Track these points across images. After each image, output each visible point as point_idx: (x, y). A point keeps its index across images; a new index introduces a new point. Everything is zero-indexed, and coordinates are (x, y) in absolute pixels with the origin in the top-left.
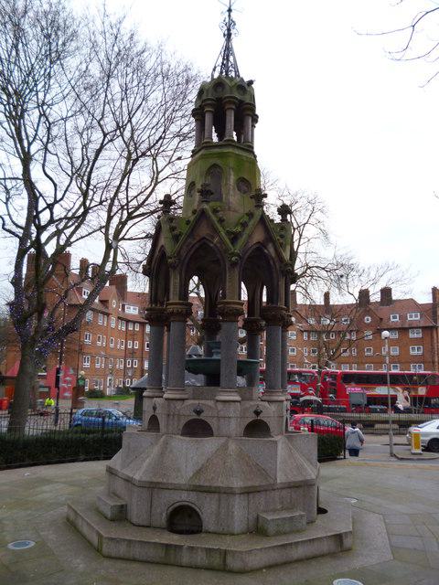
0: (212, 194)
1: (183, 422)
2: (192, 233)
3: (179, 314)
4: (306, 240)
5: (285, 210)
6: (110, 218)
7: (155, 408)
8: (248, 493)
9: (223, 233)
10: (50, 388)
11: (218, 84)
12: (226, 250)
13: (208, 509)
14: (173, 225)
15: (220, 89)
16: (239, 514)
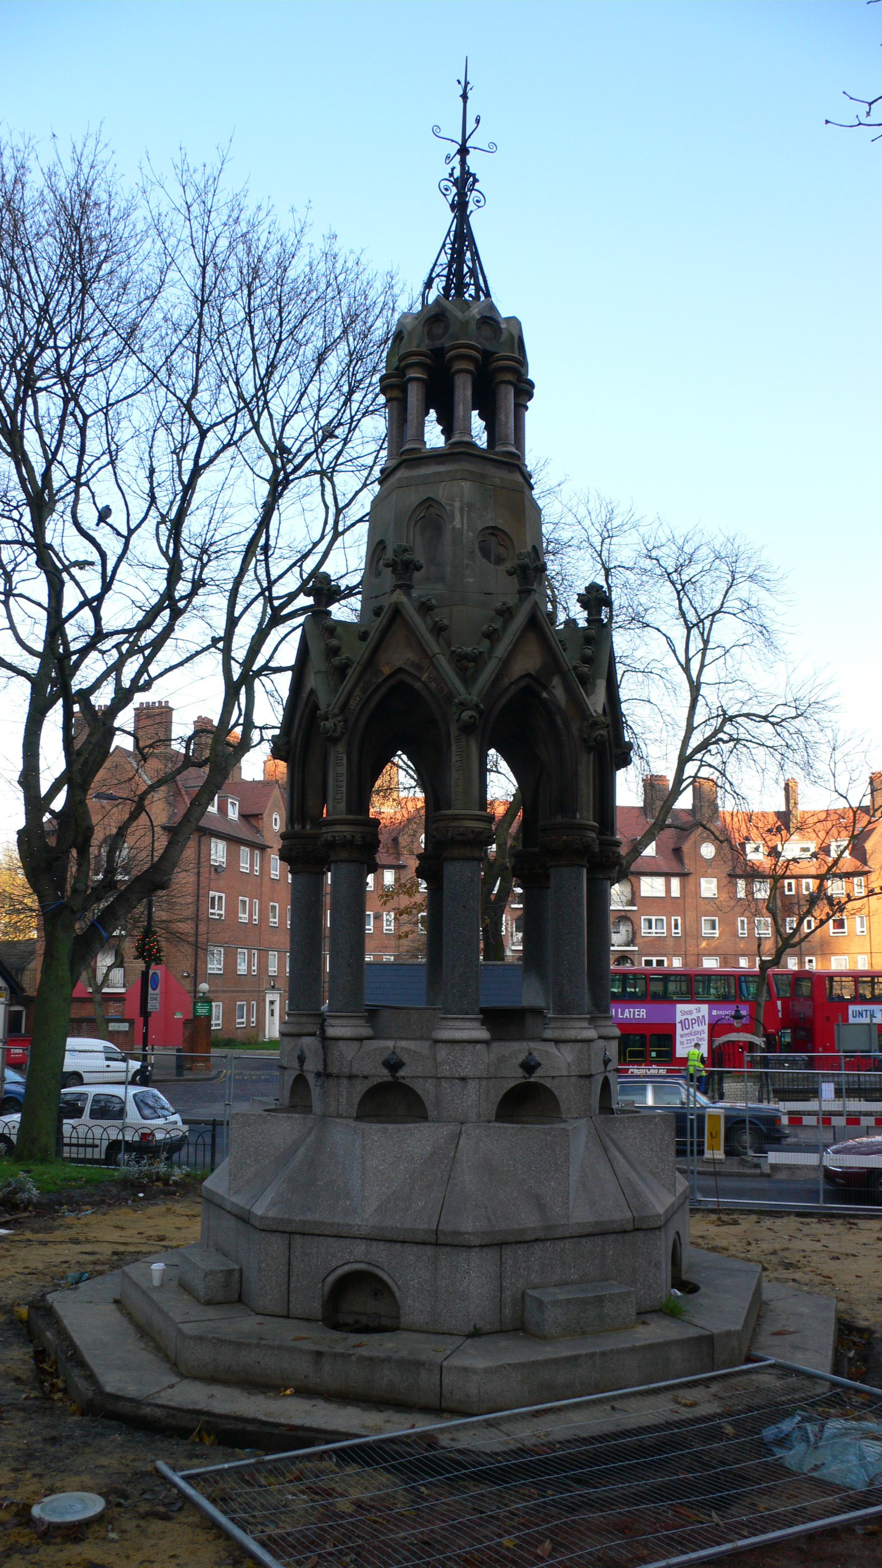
0: (418, 568)
1: (361, 1088)
2: (371, 662)
3: (347, 844)
4: (719, 652)
5: (596, 599)
6: (232, 622)
7: (301, 1059)
8: (501, 1245)
9: (443, 661)
10: (131, 1022)
11: (434, 318)
12: (450, 697)
13: (410, 1277)
14: (334, 642)
15: (438, 329)
16: (473, 1284)
